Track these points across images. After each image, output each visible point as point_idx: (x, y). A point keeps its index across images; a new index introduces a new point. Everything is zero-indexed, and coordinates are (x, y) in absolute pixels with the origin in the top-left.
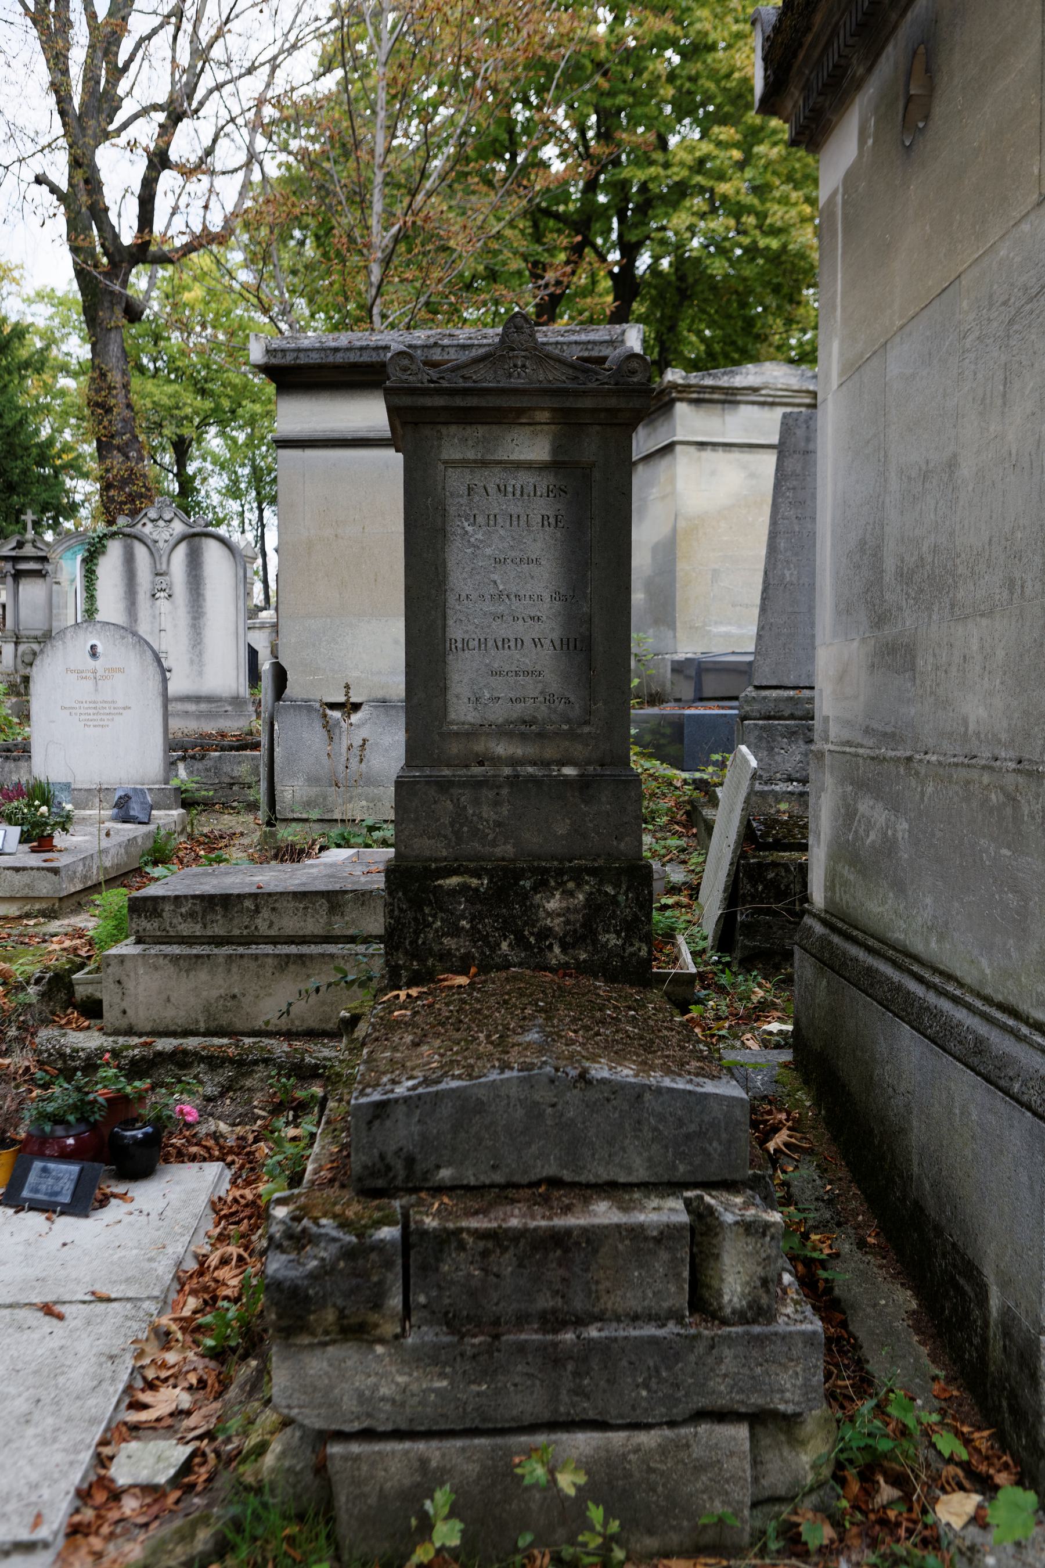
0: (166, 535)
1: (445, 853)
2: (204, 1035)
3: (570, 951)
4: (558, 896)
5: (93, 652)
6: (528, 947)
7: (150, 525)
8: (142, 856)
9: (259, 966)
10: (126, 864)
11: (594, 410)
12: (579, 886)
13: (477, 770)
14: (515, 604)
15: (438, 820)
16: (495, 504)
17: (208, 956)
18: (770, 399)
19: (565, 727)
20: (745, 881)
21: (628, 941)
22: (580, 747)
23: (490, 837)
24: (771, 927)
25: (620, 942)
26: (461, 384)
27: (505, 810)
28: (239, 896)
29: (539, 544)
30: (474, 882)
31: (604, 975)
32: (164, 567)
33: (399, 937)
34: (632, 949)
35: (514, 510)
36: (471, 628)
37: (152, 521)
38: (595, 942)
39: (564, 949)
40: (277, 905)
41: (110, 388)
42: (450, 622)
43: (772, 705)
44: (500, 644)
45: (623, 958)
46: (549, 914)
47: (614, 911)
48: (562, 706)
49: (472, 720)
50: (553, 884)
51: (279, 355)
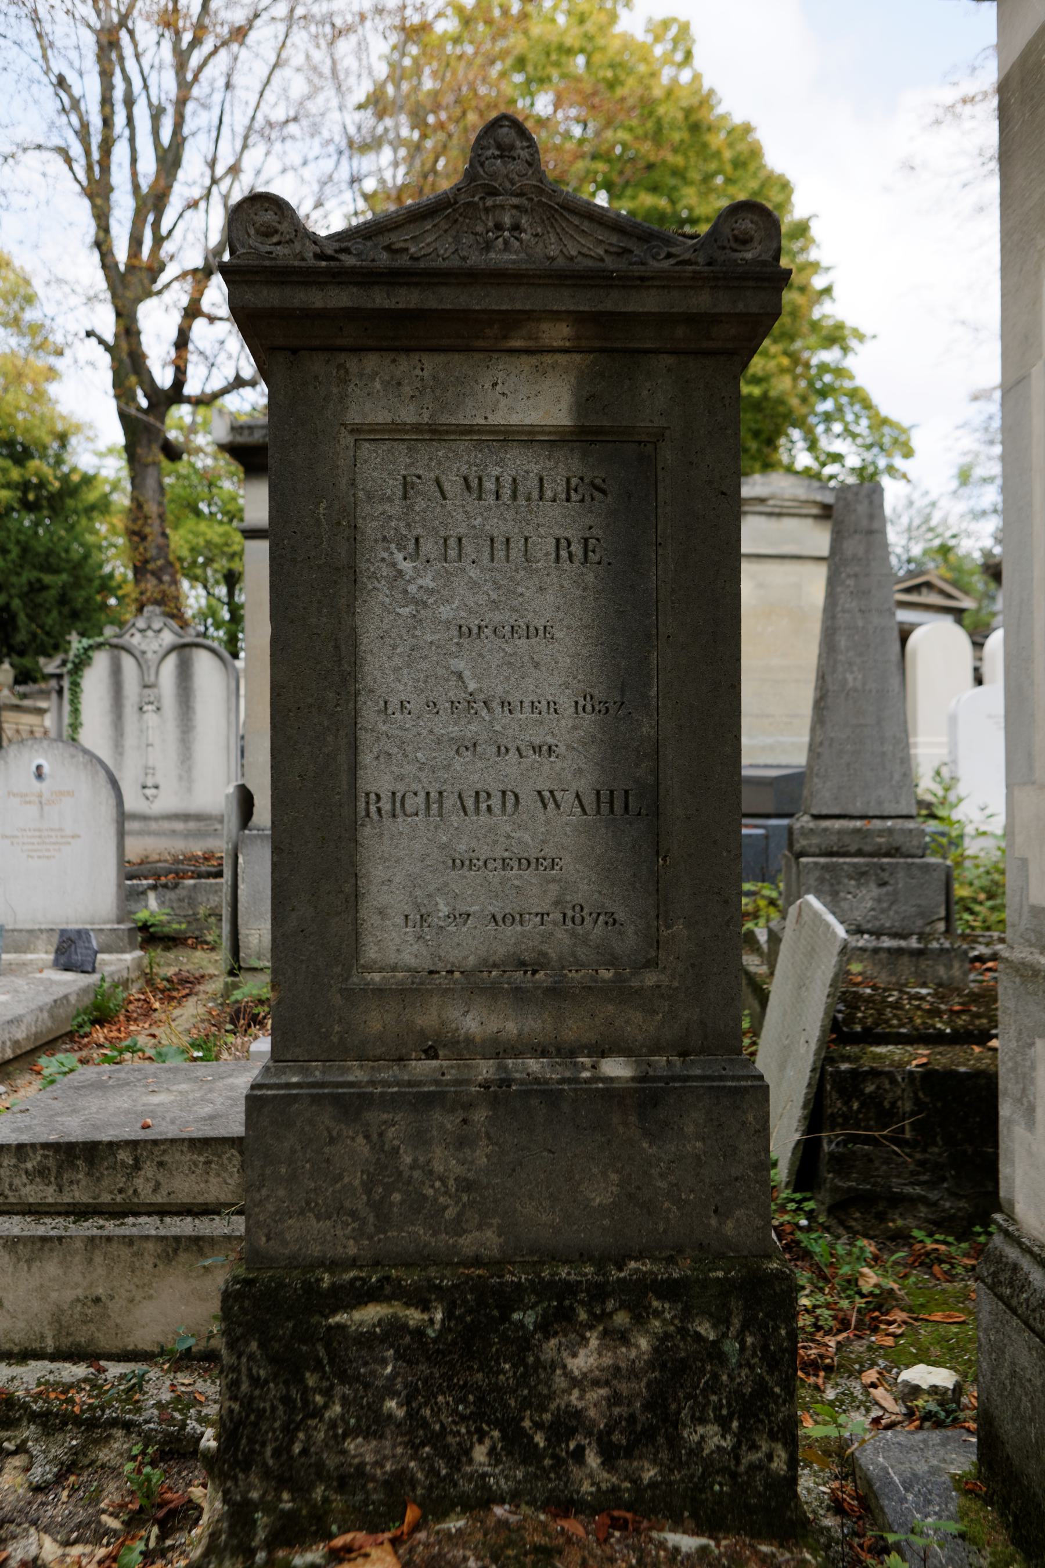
0: (155, 646)
1: (352, 1250)
2: (53, 1358)
3: (622, 1463)
4: (594, 1343)
5: (39, 773)
6: (529, 1454)
7: (138, 636)
8: (78, 1015)
9: (135, 1254)
10: (50, 1030)
11: (664, 320)
12: (639, 1320)
13: (422, 1068)
14: (502, 719)
15: (340, 1177)
16: (460, 516)
17: (60, 1239)
18: (777, 510)
19: (606, 974)
20: (835, 1095)
21: (745, 1439)
22: (637, 1017)
23: (450, 1214)
24: (871, 1161)
25: (727, 1443)
26: (384, 259)
27: (481, 1156)
28: (110, 1144)
29: (550, 598)
30: (414, 1316)
31: (694, 1515)
32: (152, 678)
33: (251, 1441)
34: (754, 1457)
35: (498, 528)
36: (409, 769)
37: (141, 631)
38: (674, 1442)
39: (609, 1456)
40: (166, 1158)
41: (146, 518)
42: (367, 758)
43: (834, 838)
44: (470, 803)
45: (734, 1475)
46: (575, 1382)
47: (715, 1377)
48: (599, 930)
49: (413, 962)
50: (583, 1316)
51: (246, 432)
